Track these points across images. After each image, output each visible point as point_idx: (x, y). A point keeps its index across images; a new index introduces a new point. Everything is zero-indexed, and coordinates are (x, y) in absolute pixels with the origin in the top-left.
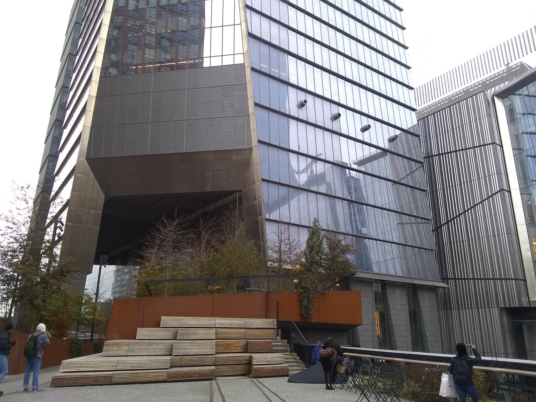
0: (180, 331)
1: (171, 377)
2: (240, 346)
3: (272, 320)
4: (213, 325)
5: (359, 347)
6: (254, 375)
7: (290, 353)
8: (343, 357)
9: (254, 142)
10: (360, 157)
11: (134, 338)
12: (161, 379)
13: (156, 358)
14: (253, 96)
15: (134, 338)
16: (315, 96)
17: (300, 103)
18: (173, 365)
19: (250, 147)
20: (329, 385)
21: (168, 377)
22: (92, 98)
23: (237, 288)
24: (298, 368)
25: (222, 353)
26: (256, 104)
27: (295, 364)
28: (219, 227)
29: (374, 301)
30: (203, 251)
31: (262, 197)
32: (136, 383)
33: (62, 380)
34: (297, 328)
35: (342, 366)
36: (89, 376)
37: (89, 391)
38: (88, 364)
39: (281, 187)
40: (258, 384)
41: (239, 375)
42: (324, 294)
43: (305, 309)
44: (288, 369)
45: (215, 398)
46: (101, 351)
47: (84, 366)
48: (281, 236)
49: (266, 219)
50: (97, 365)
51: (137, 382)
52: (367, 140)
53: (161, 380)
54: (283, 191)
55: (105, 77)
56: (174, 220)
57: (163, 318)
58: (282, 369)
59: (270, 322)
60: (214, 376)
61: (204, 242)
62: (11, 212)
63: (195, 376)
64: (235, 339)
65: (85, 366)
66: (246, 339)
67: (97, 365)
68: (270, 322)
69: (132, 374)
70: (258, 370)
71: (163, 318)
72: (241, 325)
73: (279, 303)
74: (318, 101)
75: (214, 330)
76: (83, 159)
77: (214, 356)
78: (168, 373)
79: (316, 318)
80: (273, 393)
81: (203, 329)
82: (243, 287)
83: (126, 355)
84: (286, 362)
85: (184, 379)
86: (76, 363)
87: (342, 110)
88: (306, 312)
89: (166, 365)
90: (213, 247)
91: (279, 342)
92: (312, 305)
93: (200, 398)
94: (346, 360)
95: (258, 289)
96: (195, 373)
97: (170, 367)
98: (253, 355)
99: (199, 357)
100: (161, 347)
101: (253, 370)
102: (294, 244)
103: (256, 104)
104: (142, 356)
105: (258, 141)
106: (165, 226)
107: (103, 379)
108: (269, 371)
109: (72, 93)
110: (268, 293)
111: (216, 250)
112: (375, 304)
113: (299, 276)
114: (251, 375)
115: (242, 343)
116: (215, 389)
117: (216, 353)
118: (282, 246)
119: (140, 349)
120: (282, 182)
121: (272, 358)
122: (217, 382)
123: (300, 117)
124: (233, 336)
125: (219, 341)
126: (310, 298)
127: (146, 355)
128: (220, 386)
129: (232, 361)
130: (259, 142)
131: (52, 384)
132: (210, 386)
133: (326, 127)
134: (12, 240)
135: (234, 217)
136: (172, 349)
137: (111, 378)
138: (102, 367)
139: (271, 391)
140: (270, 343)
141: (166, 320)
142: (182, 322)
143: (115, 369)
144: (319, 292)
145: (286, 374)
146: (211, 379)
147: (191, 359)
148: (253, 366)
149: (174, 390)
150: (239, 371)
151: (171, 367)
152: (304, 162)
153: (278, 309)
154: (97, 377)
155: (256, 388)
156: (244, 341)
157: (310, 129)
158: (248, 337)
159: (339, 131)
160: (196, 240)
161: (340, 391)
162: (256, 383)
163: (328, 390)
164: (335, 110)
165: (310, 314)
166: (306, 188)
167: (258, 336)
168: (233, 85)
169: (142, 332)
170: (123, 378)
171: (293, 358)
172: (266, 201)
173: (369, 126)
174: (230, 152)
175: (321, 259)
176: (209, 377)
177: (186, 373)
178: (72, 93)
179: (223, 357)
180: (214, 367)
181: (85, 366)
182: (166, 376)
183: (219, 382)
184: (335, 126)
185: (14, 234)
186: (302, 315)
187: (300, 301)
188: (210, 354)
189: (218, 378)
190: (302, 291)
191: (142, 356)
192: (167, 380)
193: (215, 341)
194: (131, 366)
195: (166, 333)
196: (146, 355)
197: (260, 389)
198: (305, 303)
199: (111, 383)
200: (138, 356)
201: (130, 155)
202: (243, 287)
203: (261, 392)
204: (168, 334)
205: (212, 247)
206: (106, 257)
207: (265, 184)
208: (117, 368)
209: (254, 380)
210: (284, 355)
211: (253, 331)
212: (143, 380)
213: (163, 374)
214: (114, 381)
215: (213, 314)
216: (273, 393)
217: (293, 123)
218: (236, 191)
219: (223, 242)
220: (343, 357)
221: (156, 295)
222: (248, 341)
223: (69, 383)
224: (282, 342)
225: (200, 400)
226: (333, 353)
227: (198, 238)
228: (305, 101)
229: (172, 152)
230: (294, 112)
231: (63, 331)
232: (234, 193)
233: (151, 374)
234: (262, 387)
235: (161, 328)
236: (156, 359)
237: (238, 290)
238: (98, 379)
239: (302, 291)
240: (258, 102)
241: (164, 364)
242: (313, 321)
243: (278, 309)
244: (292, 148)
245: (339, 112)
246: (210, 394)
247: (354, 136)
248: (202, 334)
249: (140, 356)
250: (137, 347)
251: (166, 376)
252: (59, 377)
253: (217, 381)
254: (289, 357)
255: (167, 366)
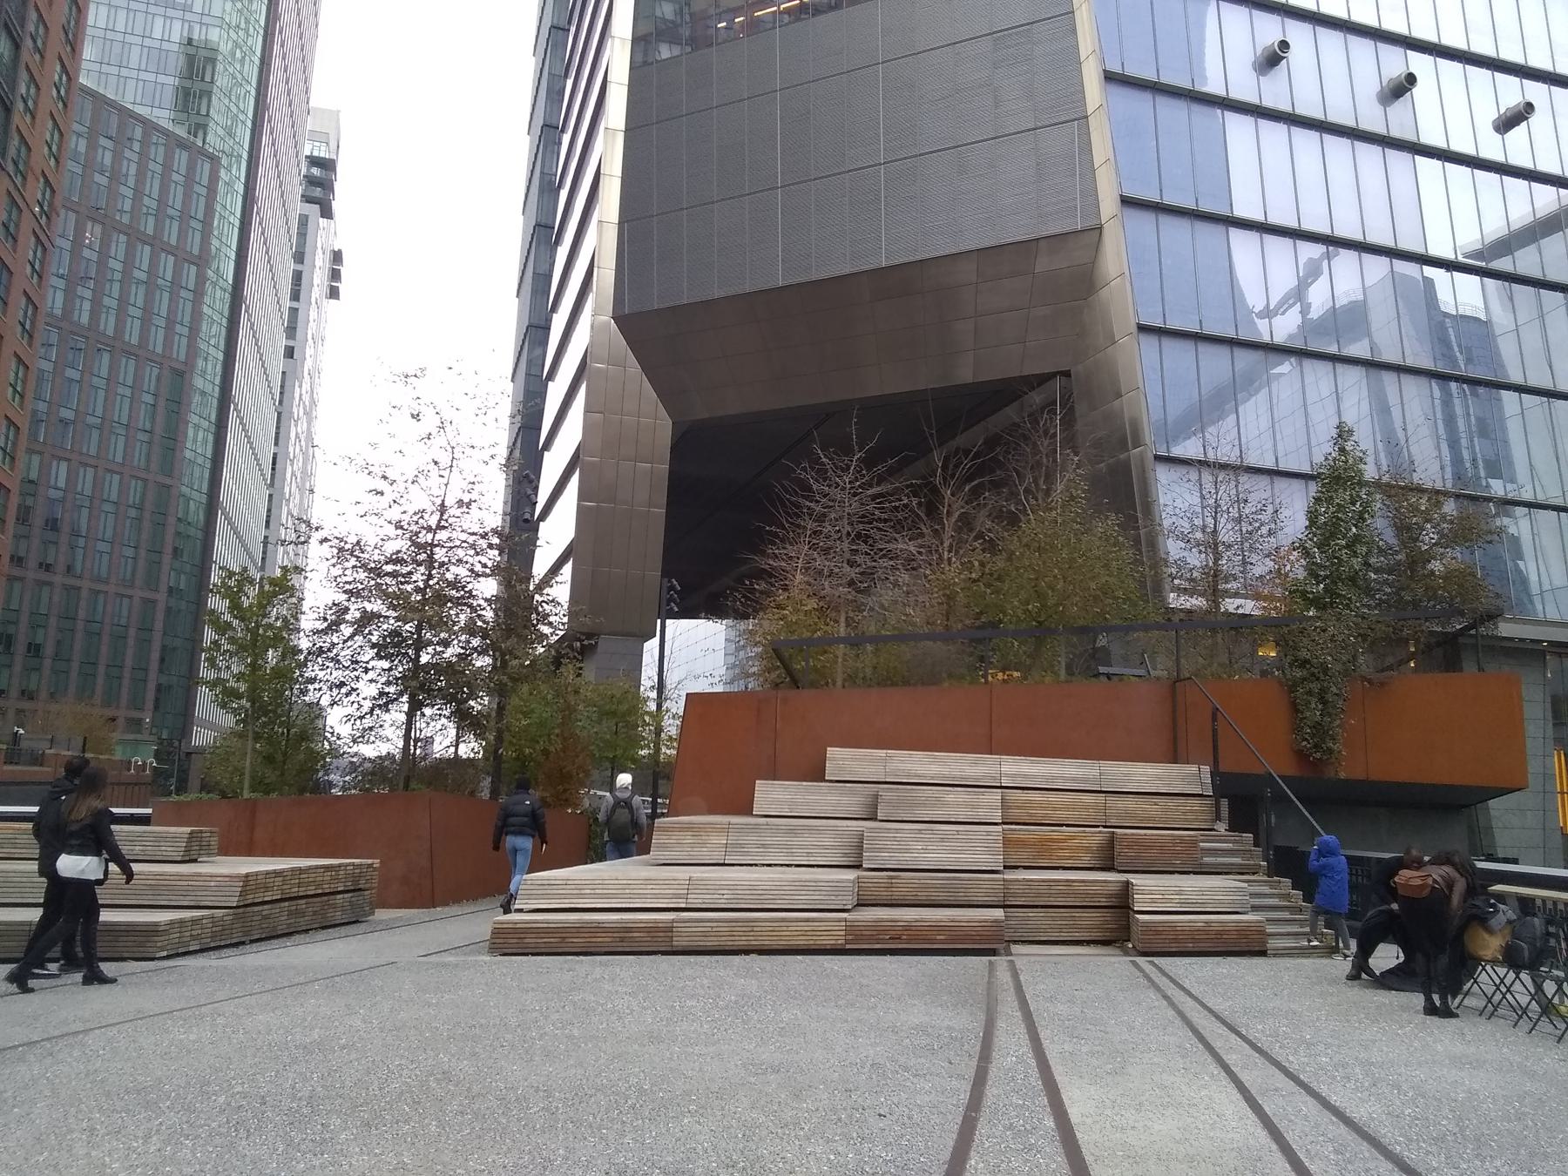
0: (886, 793)
1: (856, 941)
2: (1087, 849)
3: (1194, 768)
4: (994, 778)
5: (1515, 861)
6: (1140, 946)
7: (1266, 878)
8: (1492, 901)
9: (1108, 205)
10: (1495, 227)
11: (747, 810)
12: (827, 941)
13: (812, 873)
14: (1098, 51)
15: (747, 810)
16: (1319, 25)
17: (1265, 54)
18: (866, 897)
19: (1091, 223)
20: (1436, 998)
21: (851, 937)
22: (614, 135)
23: (1069, 668)
24: (1301, 930)
25: (1026, 868)
26: (1110, 78)
27: (1286, 915)
28: (998, 472)
29: (1549, 715)
30: (950, 552)
31: (1141, 387)
32: (747, 952)
33: (522, 936)
34: (1292, 795)
35: (1490, 931)
36: (601, 925)
37: (598, 972)
38: (600, 886)
39: (1206, 350)
40: (1157, 980)
41: (1088, 943)
42: (1382, 684)
43: (1313, 736)
44: (1262, 933)
45: (1001, 1024)
46: (645, 849)
47: (588, 891)
48: (1217, 493)
49: (1158, 458)
50: (627, 891)
51: (751, 948)
52: (1521, 160)
53: (828, 947)
54: (1216, 363)
55: (645, 63)
56: (849, 452)
57: (832, 752)
58: (1243, 932)
59: (1191, 776)
60: (1001, 941)
61: (949, 524)
62: (374, 445)
63: (938, 937)
64: (1068, 825)
65: (592, 892)
66: (1105, 827)
67: (627, 891)
68: (1191, 776)
69: (734, 924)
70: (1150, 929)
71: (832, 752)
72: (1085, 780)
73: (1219, 715)
74: (1331, 40)
75: (996, 795)
76: (606, 318)
77: (1001, 876)
78: (848, 924)
79: (1349, 766)
80: (1217, 1017)
81: (959, 789)
82: (1090, 663)
83: (722, 862)
84: (1255, 908)
85: (900, 946)
86: (564, 882)
87: (1420, 63)
88: (1316, 746)
89: (840, 898)
90: (980, 536)
91: (1223, 841)
92: (1338, 722)
93: (947, 1023)
94: (1507, 913)
95: (1142, 672)
96: (938, 928)
97: (858, 905)
98: (1135, 879)
99: (948, 879)
100: (827, 842)
101: (1134, 928)
102: (1264, 517)
103: (1110, 78)
104: (770, 865)
105: (1122, 201)
106: (822, 474)
107: (645, 935)
108: (1194, 933)
109: (566, 138)
110: (1176, 682)
111: (991, 547)
112: (1554, 724)
113: (1287, 626)
114: (1130, 946)
115: (1096, 837)
116: (1006, 991)
117: (1005, 867)
118: (1221, 525)
119: (764, 846)
120: (1209, 329)
121: (1202, 892)
122: (1012, 961)
123: (1268, 103)
124: (1062, 815)
125: (1015, 830)
126: (1329, 697)
127: (782, 865)
128: (1021, 978)
129: (1067, 895)
130: (1127, 202)
131: (493, 946)
132: (987, 974)
133: (1365, 125)
134: (391, 530)
135: (1046, 433)
136: (860, 847)
137: (670, 934)
138: (644, 896)
139: (1210, 1011)
140: (1194, 843)
141: (840, 759)
142: (892, 766)
143: (683, 906)
144: (1364, 678)
145: (1257, 949)
146: (993, 952)
147: (922, 881)
148: (1138, 916)
149: (865, 982)
150: (1089, 929)
151: (858, 905)
152: (1284, 261)
153: (1215, 732)
154: (627, 929)
155: (1152, 994)
156: (1100, 832)
157: (1306, 140)
158: (1113, 822)
159: (1409, 136)
160: (925, 518)
161: (1484, 1027)
162: (1151, 975)
163: (1432, 1017)
164: (1395, 62)
165: (1330, 751)
166: (1299, 344)
167: (1149, 819)
168: (1028, 24)
169: (770, 794)
170: (705, 934)
171: (1280, 896)
172: (1156, 414)
173: (1529, 107)
174: (1027, 248)
175: (1367, 564)
176: (985, 945)
177: (908, 928)
178: (566, 138)
179: (1031, 880)
180: (999, 913)
181: (592, 892)
182: (843, 933)
183: (1019, 963)
184: (1397, 122)
185: (395, 514)
186: (1301, 756)
187: (1295, 708)
188: (984, 868)
189: (1015, 948)
190: (1299, 673)
191: (770, 865)
192: (848, 947)
193: (999, 828)
194: (732, 896)
195: (845, 800)
196: (782, 865)
197: (1166, 997)
198: (1314, 712)
199: (669, 949)
200: (756, 865)
201: (730, 294)
202: (1090, 663)
203: (1171, 1013)
204: (849, 801)
205: (976, 538)
206: (675, 583)
207: (1149, 344)
208: (689, 901)
209: (1141, 960)
210: (1246, 885)
211: (1130, 803)
212: (767, 942)
213: (831, 928)
214: (679, 942)
215: (990, 746)
216: (1217, 1017)
217: (1238, 127)
218: (1053, 375)
219: (1013, 521)
220: (1492, 901)
221: (813, 685)
222: (1113, 833)
223: (543, 945)
224: (1234, 842)
225: (949, 1028)
226: (1450, 884)
227: (932, 510)
228: (1284, 45)
229: (847, 270)
230: (1244, 87)
231: (565, 791)
232: (1050, 379)
233: (794, 927)
234: (1172, 991)
235: (828, 784)
236: (807, 877)
237: (1070, 671)
238: (631, 935)
239: (1299, 673)
240: (1117, 68)
241: (837, 893)
242: (1342, 775)
243: (1215, 732)
244: (1241, 211)
245: (1412, 70)
246: (984, 1007)
247: (1466, 148)
248: (958, 805)
249: (763, 865)
250: (752, 839)
251: (843, 933)
252: (510, 926)
253: (1009, 958)
254: (1266, 889)
255: (844, 902)
